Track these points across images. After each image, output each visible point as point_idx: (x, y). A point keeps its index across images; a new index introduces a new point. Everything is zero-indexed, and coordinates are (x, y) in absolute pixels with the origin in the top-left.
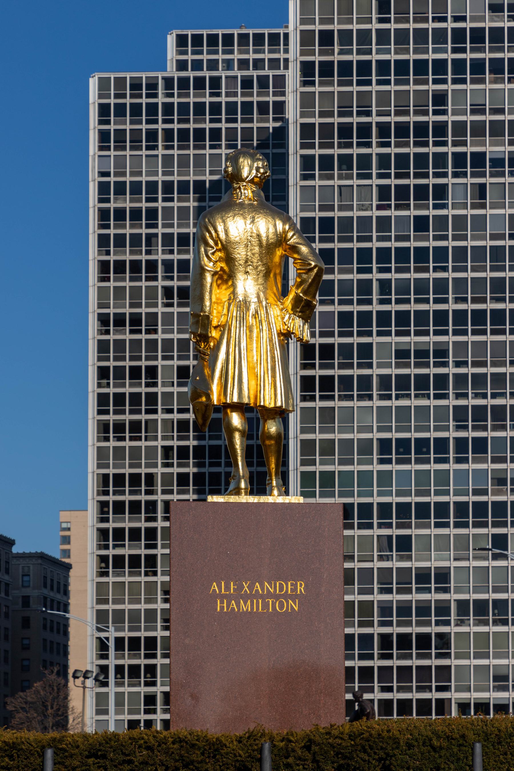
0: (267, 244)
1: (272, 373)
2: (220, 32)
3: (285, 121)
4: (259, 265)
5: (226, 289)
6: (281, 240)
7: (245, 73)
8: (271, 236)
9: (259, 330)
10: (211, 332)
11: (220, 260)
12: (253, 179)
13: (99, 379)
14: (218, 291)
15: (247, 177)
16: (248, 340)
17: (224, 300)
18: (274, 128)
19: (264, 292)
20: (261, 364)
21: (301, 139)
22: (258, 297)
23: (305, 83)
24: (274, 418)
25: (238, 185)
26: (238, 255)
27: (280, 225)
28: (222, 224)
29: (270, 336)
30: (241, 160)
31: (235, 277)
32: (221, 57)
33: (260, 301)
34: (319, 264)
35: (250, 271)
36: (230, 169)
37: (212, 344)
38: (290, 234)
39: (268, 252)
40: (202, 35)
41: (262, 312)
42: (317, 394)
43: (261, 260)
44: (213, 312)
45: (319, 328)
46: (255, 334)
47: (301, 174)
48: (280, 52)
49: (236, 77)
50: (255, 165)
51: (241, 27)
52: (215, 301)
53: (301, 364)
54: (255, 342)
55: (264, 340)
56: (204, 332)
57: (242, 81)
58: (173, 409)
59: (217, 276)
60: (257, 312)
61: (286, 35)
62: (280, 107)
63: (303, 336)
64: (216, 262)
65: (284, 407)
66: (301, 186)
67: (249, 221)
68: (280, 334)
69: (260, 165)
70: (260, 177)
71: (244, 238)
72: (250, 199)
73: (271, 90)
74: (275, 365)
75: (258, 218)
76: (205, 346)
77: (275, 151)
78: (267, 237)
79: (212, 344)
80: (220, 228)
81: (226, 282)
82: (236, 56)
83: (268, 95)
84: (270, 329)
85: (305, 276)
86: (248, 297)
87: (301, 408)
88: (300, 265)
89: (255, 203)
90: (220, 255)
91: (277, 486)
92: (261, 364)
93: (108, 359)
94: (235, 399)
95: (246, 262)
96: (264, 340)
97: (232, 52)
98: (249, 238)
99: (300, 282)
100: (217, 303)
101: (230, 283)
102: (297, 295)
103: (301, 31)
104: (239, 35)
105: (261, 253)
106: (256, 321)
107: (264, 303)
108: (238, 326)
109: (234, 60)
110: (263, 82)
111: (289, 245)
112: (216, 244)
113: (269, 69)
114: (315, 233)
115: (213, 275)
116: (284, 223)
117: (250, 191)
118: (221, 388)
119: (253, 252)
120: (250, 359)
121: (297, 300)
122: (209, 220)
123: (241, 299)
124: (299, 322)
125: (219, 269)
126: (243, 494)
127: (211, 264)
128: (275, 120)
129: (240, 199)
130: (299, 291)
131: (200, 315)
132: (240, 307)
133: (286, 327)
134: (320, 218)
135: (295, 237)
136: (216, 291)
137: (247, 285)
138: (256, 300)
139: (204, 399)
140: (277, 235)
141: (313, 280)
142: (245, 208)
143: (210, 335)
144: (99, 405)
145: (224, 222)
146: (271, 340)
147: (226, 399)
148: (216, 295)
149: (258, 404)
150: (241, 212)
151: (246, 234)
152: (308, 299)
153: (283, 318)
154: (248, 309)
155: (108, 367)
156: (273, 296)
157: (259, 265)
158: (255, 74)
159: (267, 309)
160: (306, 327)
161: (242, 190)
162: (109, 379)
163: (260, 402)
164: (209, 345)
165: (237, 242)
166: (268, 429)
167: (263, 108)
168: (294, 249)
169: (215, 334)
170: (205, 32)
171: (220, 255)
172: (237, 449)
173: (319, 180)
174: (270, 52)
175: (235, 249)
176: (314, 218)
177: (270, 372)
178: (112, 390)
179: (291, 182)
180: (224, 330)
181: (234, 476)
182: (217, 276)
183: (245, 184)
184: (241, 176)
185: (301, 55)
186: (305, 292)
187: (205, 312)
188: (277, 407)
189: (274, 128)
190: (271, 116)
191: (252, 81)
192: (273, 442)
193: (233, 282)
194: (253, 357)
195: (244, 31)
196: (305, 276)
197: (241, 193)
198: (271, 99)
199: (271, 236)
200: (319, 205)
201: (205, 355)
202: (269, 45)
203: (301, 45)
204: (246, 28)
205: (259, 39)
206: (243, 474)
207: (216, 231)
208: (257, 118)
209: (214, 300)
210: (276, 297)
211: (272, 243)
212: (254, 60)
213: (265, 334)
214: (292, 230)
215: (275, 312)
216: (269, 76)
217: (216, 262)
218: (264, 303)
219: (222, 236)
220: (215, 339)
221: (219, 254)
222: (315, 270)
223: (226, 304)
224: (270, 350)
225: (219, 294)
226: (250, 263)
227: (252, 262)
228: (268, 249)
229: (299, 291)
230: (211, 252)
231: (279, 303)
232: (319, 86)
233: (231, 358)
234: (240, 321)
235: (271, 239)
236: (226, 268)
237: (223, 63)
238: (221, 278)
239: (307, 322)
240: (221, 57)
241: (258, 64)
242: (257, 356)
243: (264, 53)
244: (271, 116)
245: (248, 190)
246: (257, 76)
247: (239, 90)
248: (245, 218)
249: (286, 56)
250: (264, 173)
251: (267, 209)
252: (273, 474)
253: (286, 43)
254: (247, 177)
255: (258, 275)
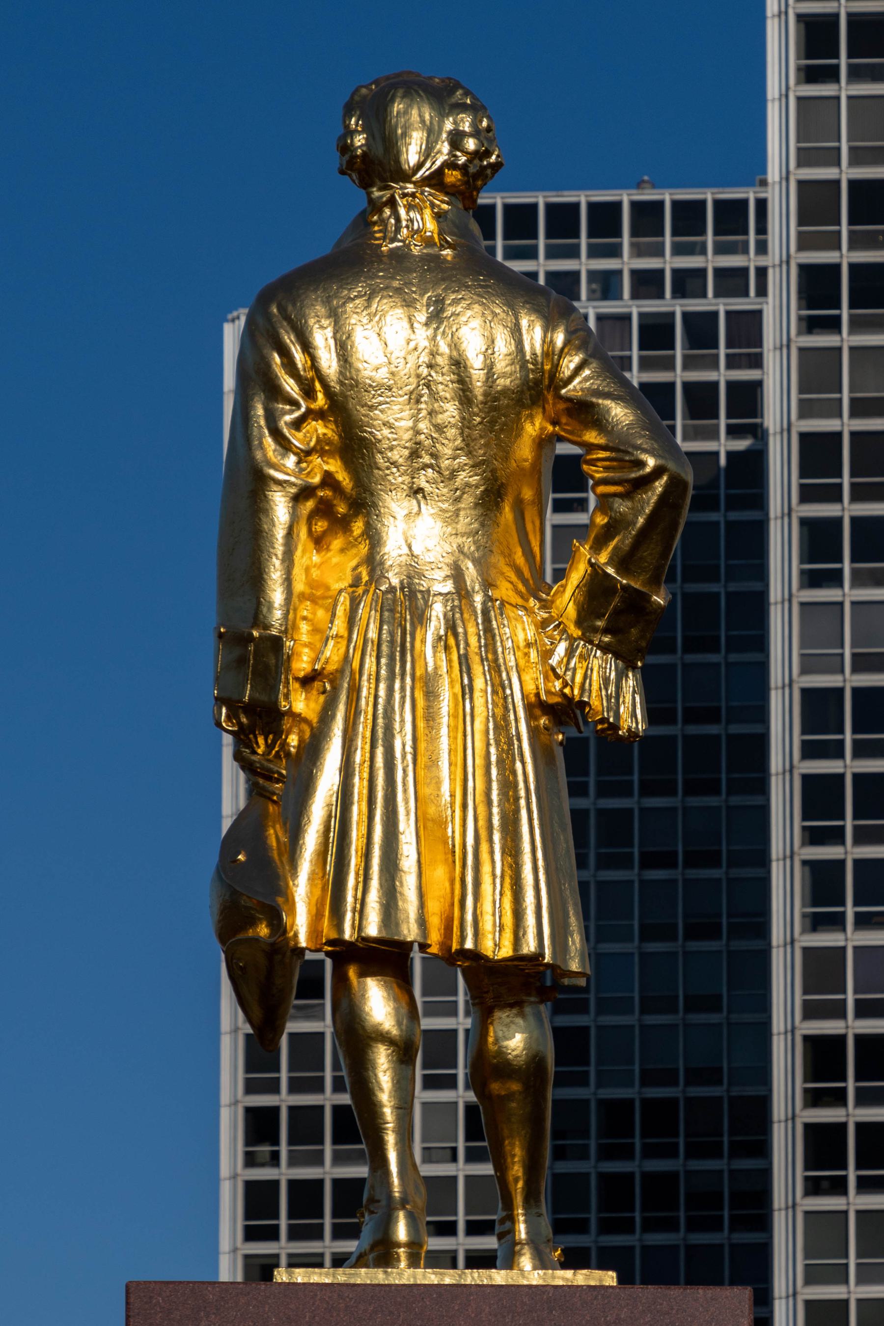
0: (486, 394)
1: (503, 838)
2: (583, 198)
3: (758, 433)
4: (461, 468)
5: (342, 550)
6: (537, 386)
7: (652, 306)
8: (501, 365)
9: (458, 689)
10: (287, 696)
11: (320, 449)
12: (440, 172)
13: (248, 1142)
14: (316, 558)
15: (420, 165)
16: (421, 724)
17: (337, 586)
18: (730, 455)
19: (476, 562)
20: (464, 806)
21: (802, 475)
22: (457, 575)
23: (811, 325)
24: (517, 1005)
25: (387, 194)
26: (386, 432)
27: (534, 335)
28: (325, 322)
29: (499, 711)
30: (398, 107)
31: (375, 505)
32: (584, 265)
33: (462, 592)
34: (671, 465)
35: (427, 488)
36: (359, 140)
37: (293, 740)
38: (570, 363)
39: (493, 422)
40: (534, 207)
41: (472, 630)
42: (852, 1175)
43: (468, 448)
44: (295, 627)
45: (856, 991)
46: (445, 705)
47: (802, 572)
48: (746, 251)
49: (627, 317)
50: (449, 125)
51: (639, 185)
52: (304, 584)
53: (806, 1091)
54: (444, 731)
55: (479, 725)
56: (264, 698)
57: (642, 328)
58: (454, 1224)
59: (310, 504)
60: (451, 627)
61: (762, 205)
62: (747, 398)
63: (617, 715)
64: (308, 453)
65: (548, 959)
66: (802, 604)
67: (421, 316)
68: (536, 706)
69: (466, 127)
70: (464, 168)
71: (405, 370)
72: (428, 242)
73: (722, 351)
74: (517, 811)
75: (456, 302)
76: (269, 747)
77: (734, 516)
78: (489, 368)
79: (293, 740)
80: (322, 338)
81: (342, 524)
82: (627, 262)
83: (715, 366)
84: (499, 687)
85: (622, 507)
86: (421, 575)
87: (807, 1213)
88: (606, 469)
89: (447, 253)
90: (322, 430)
91: (533, 1241)
92: (464, 806)
93: (273, 1087)
94: (372, 929)
95: (414, 454)
96: (479, 725)
97: (615, 252)
98: (424, 371)
99: (607, 526)
100: (314, 600)
101: (358, 527)
102: (596, 576)
103: (801, 183)
104: (634, 205)
105: (465, 425)
106: (449, 661)
107: (478, 599)
108: (383, 672)
109: (620, 272)
110: (701, 330)
111: (568, 400)
112: (309, 393)
113: (717, 295)
114: (842, 731)
115: (297, 499)
116: (549, 327)
117: (427, 213)
118: (324, 889)
119: (440, 419)
120: (425, 791)
121: (597, 589)
122: (282, 309)
123: (395, 582)
124: (601, 665)
125: (316, 480)
126: (403, 1264)
127: (291, 461)
128: (733, 432)
129: (393, 240)
130: (603, 558)
131: (251, 638)
132: (392, 611)
133: (558, 684)
134: (856, 691)
135: (587, 372)
136: (307, 557)
137: (420, 533)
138: (448, 587)
139: (263, 930)
140: (523, 363)
141: (652, 519)
142: (410, 271)
143: (284, 705)
144: (248, 1216)
145: (336, 317)
146: (502, 726)
147: (338, 924)
148: (307, 570)
149: (455, 946)
150: (396, 284)
151: (411, 359)
152: (637, 586)
153: (547, 654)
154: (420, 618)
155: (276, 1110)
156: (514, 578)
157: (461, 468)
158: (680, 308)
159: (487, 620)
160: (630, 682)
161: (402, 212)
162: (276, 1142)
163: (463, 938)
164: (285, 744)
165: (381, 386)
166: (497, 1041)
167: (701, 400)
168: (583, 411)
169: (302, 703)
170: (541, 199)
171: (322, 430)
172: (381, 1105)
173: (853, 585)
174: (720, 249)
175: (372, 408)
176: (840, 691)
177: (497, 837)
178: (284, 1173)
179: (775, 592)
180: (336, 689)
181: (372, 1200)
182: (310, 504)
183: (410, 188)
184: (398, 161)
185: (801, 247)
186: (623, 562)
187: (267, 627)
188: (523, 958)
189: (730, 455)
190: (723, 421)
191: (672, 327)
192: (515, 1087)
193: (368, 526)
194: (438, 784)
195: (648, 195)
196: (622, 507)
197: (398, 220)
198: (722, 375)
199: (501, 365)
200: (854, 656)
201: (269, 778)
202: (716, 233)
203: (801, 222)
204: (654, 186)
205: (689, 216)
206: (404, 1192)
207: (307, 347)
208: (684, 427)
209: (299, 586)
210: (525, 582)
211: (505, 391)
212: (676, 272)
213: (482, 701)
214: (578, 349)
215: (519, 630)
216: (715, 314)
217: (308, 453)
218: (478, 599)
219: (329, 363)
220: (305, 720)
221: (319, 428)
222: (659, 486)
223: (344, 603)
224: (500, 762)
225: (319, 566)
226: (427, 459)
227: (432, 455)
228: (493, 412)
229: (603, 558)
230: (288, 418)
231: (532, 602)
232: (851, 332)
233: (359, 785)
234: (391, 658)
235: (504, 375)
236: (343, 477)
237: (590, 281)
238: (324, 510)
239: (634, 668)
240: (584, 265)
241: (688, 283)
242: (452, 780)
243: (703, 252)
244: (723, 421)
245: (421, 211)
246: (685, 315)
247: (635, 353)
248: (409, 304)
249: (762, 261)
250: (477, 155)
251: (489, 275)
252: (519, 1200)
253: (762, 229)
254: (420, 165)
255: (458, 500)
